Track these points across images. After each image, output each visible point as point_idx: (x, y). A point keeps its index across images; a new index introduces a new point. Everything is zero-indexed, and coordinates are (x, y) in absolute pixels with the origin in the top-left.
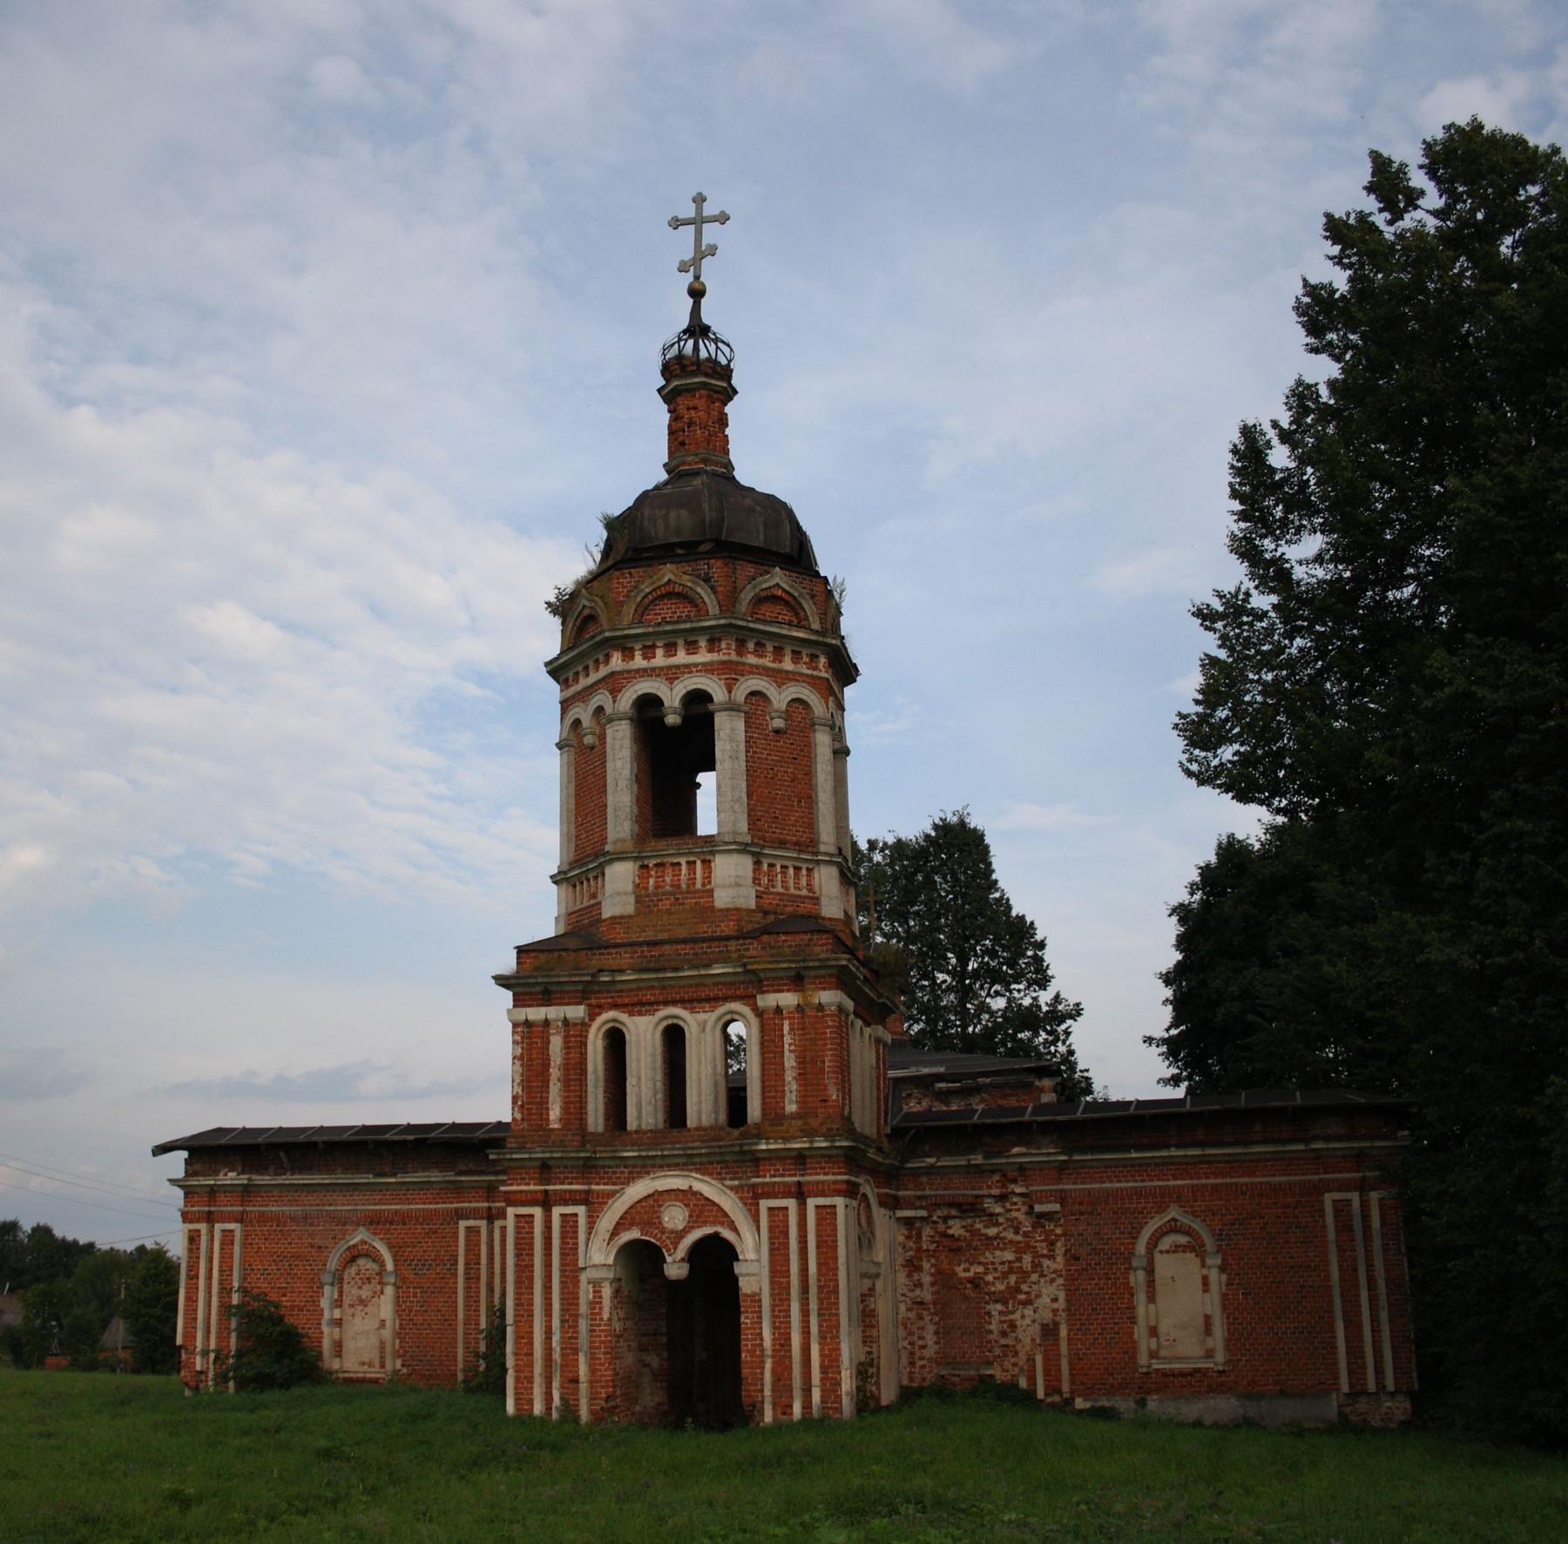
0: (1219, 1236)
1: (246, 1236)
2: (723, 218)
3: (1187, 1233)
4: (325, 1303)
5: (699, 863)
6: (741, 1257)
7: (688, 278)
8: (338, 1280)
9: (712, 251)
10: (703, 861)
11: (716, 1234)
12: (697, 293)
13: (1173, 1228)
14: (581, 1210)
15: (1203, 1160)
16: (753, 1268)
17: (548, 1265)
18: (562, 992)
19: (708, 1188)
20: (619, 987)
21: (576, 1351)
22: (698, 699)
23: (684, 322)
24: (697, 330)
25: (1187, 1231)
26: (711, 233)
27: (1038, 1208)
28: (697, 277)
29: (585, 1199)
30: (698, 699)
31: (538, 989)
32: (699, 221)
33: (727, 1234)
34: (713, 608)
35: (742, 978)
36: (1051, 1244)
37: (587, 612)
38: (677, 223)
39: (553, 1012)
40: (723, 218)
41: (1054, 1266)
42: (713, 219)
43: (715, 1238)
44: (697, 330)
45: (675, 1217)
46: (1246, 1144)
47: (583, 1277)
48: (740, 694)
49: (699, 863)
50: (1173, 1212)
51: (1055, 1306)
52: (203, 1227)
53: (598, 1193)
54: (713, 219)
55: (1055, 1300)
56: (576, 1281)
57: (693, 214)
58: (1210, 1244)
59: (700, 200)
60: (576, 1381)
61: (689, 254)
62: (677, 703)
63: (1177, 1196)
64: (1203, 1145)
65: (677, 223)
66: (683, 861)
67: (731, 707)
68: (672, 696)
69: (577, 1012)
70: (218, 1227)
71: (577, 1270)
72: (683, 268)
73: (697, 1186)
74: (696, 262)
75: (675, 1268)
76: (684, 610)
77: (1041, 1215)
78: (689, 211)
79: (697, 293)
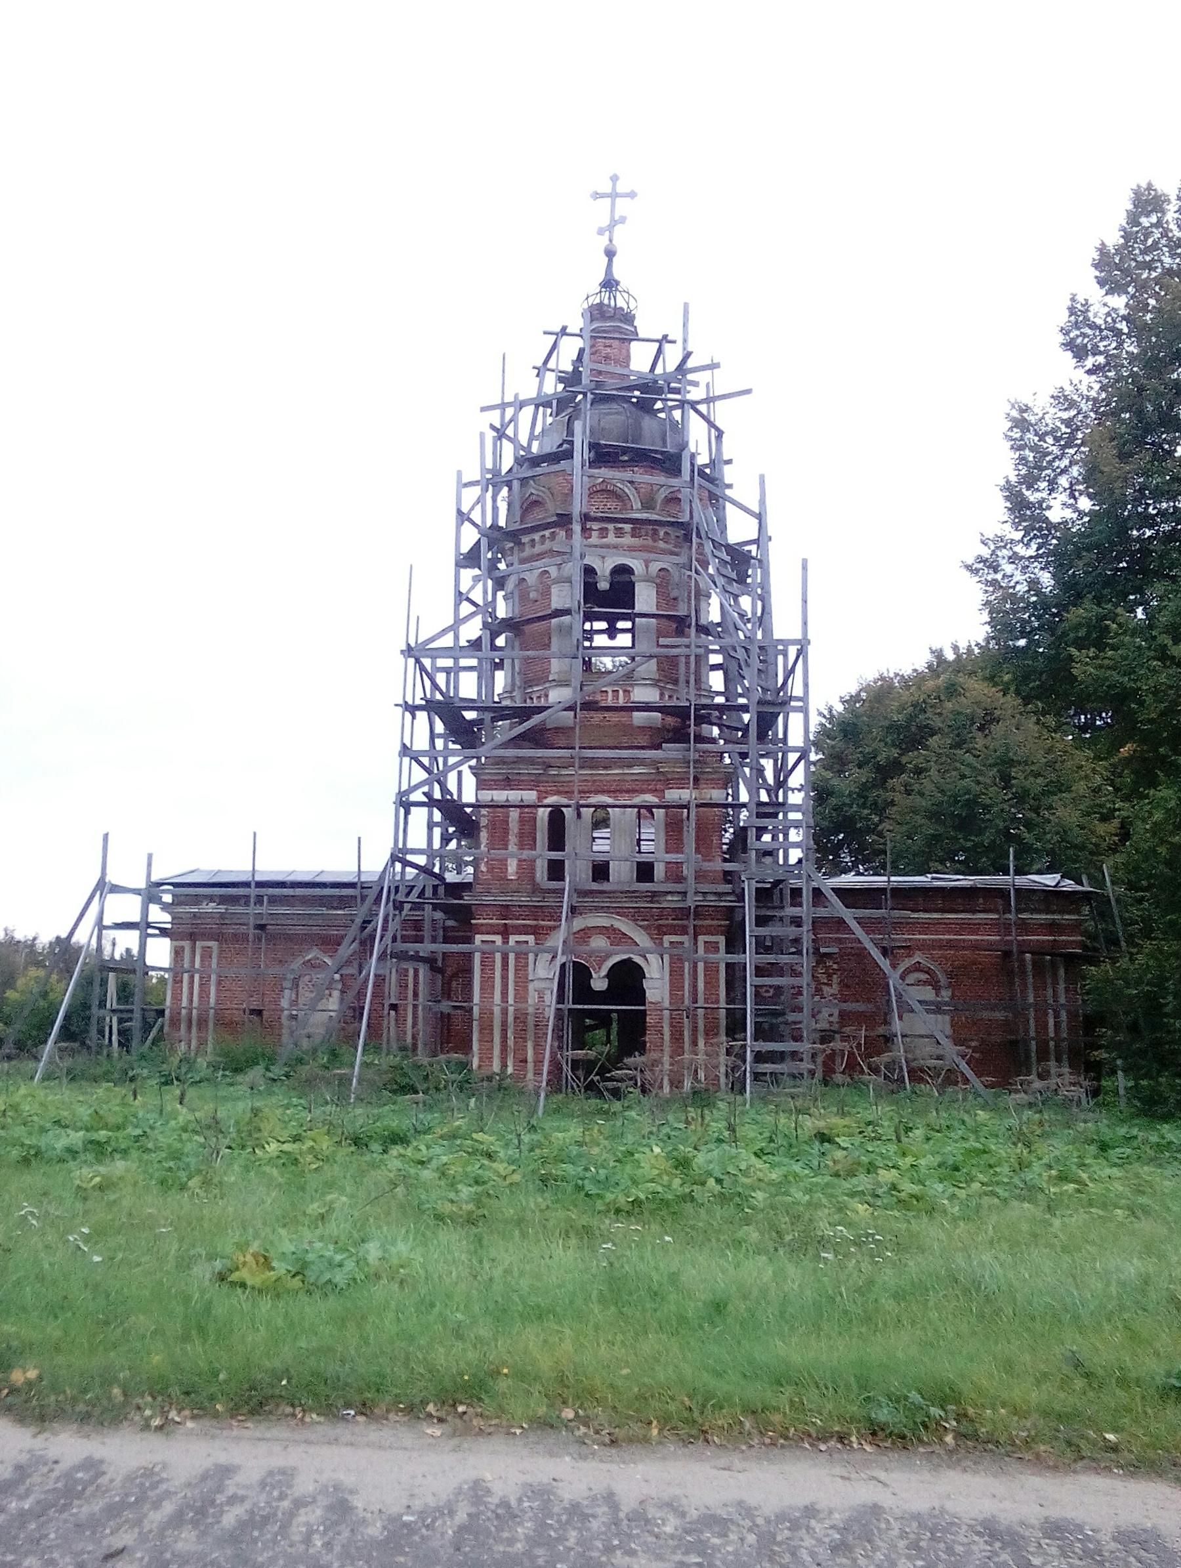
0: (950, 975)
1: (221, 951)
2: (632, 195)
3: (927, 972)
4: (285, 1003)
5: (621, 692)
6: (647, 975)
7: (604, 241)
8: (296, 984)
9: (623, 220)
10: (625, 691)
11: (630, 959)
12: (610, 254)
13: (917, 968)
14: (531, 939)
15: (938, 922)
16: (657, 984)
17: (505, 978)
18: (519, 781)
19: (623, 925)
20: (562, 779)
21: (525, 1040)
22: (622, 571)
23: (601, 277)
24: (609, 284)
25: (928, 971)
26: (622, 206)
27: (822, 950)
28: (611, 241)
29: (535, 931)
30: (622, 571)
31: (501, 777)
32: (614, 196)
33: (638, 959)
34: (637, 505)
35: (653, 777)
36: (829, 976)
37: (534, 498)
38: (597, 196)
39: (514, 796)
40: (632, 195)
41: (832, 991)
42: (603, 196)
43: (629, 962)
44: (609, 284)
45: (599, 943)
46: (974, 912)
47: (531, 986)
48: (655, 567)
49: (621, 692)
50: (918, 957)
51: (831, 1019)
52: (186, 944)
53: (543, 927)
54: (603, 196)
55: (831, 1015)
56: (526, 988)
57: (609, 190)
58: (943, 980)
59: (614, 179)
60: (525, 1061)
61: (605, 222)
62: (608, 572)
63: (923, 946)
64: (943, 911)
65: (597, 196)
66: (609, 690)
67: (647, 579)
68: (604, 567)
69: (530, 796)
70: (701, 939)
71: (527, 981)
72: (601, 232)
73: (617, 925)
74: (611, 228)
75: (599, 983)
76: (612, 504)
77: (826, 955)
78: (608, 189)
79: (610, 254)
